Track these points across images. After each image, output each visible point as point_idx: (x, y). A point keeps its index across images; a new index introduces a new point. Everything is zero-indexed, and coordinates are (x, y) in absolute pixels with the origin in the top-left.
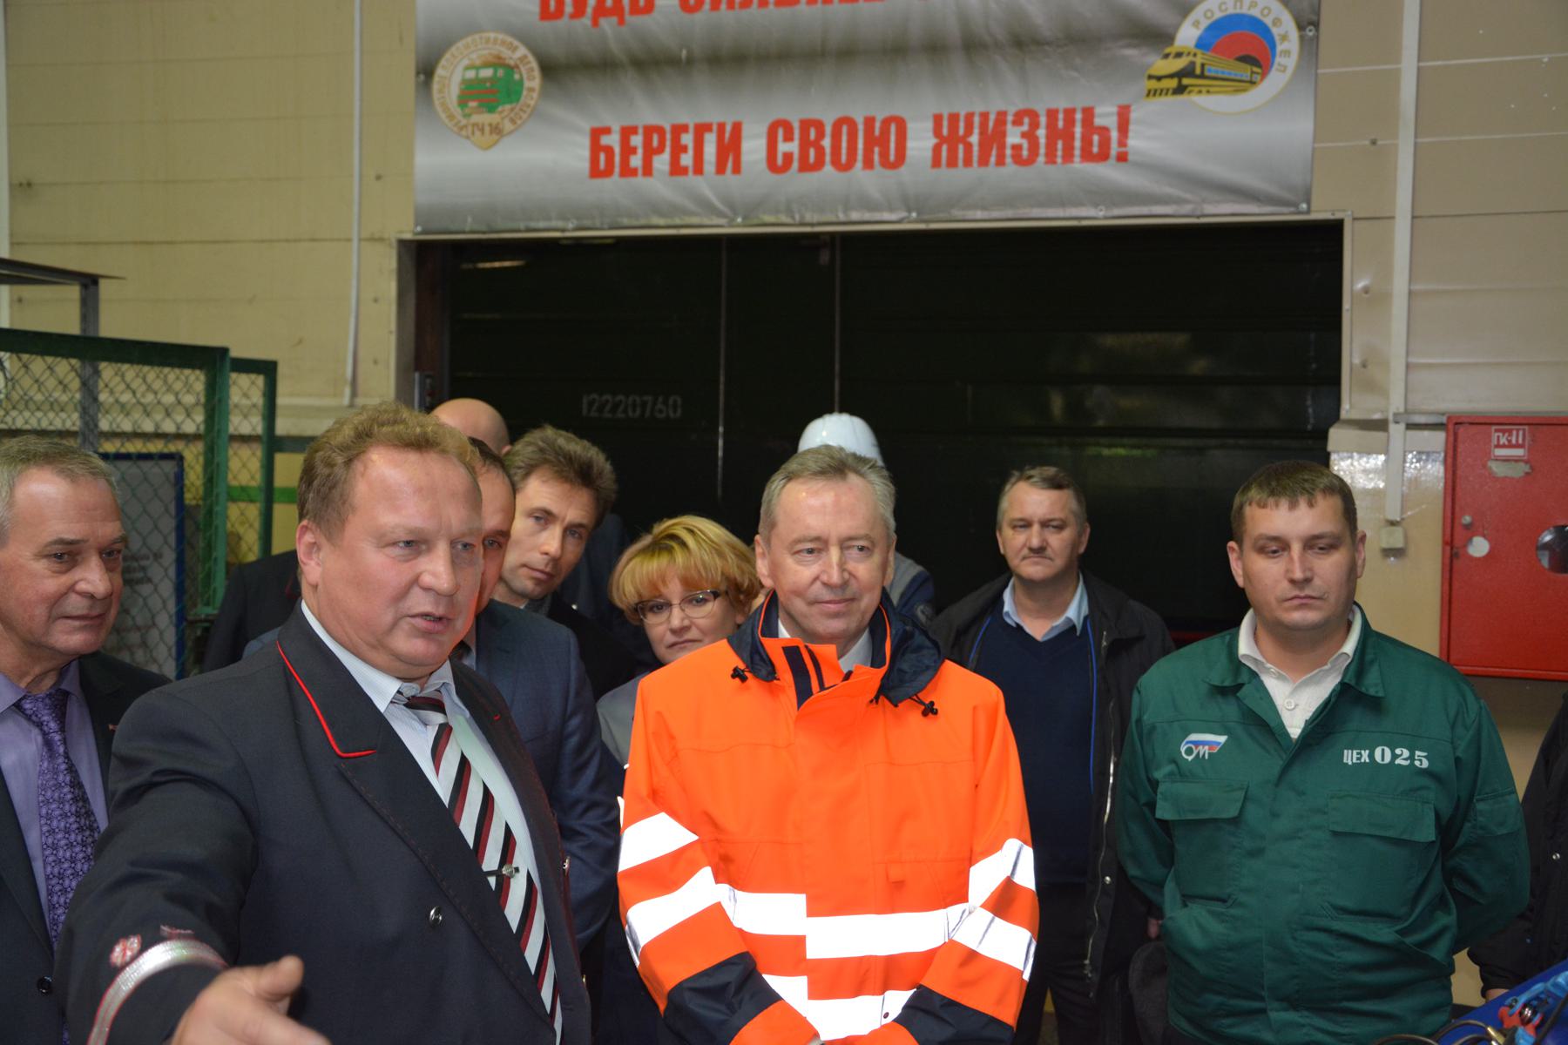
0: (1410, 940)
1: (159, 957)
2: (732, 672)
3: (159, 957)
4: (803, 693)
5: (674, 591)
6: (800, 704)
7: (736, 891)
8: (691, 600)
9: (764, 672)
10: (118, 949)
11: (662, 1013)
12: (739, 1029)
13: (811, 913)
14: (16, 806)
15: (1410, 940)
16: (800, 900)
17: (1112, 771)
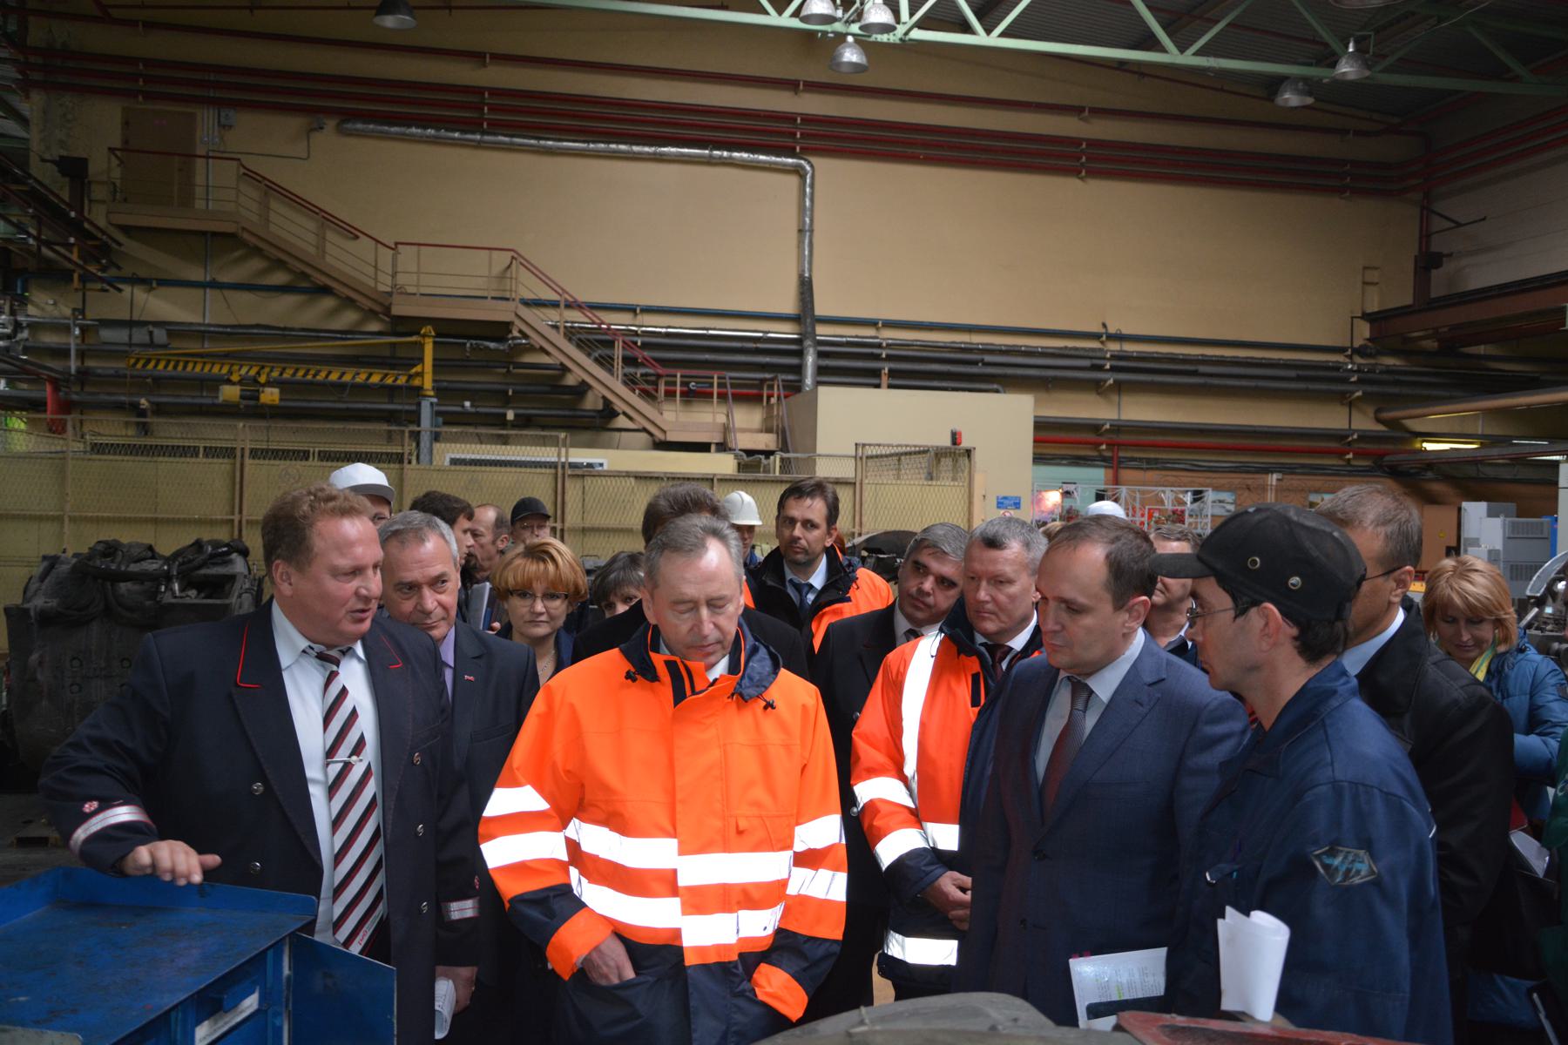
0: (983, 701)
1: (123, 814)
2: (625, 674)
3: (123, 814)
4: (679, 696)
5: (539, 588)
6: (676, 704)
7: (1422, 594)
8: (549, 596)
9: (650, 677)
10: (87, 806)
11: (507, 909)
12: (557, 929)
13: (682, 852)
14: (1098, 717)
15: (983, 701)
16: (672, 843)
17: (736, 154)
